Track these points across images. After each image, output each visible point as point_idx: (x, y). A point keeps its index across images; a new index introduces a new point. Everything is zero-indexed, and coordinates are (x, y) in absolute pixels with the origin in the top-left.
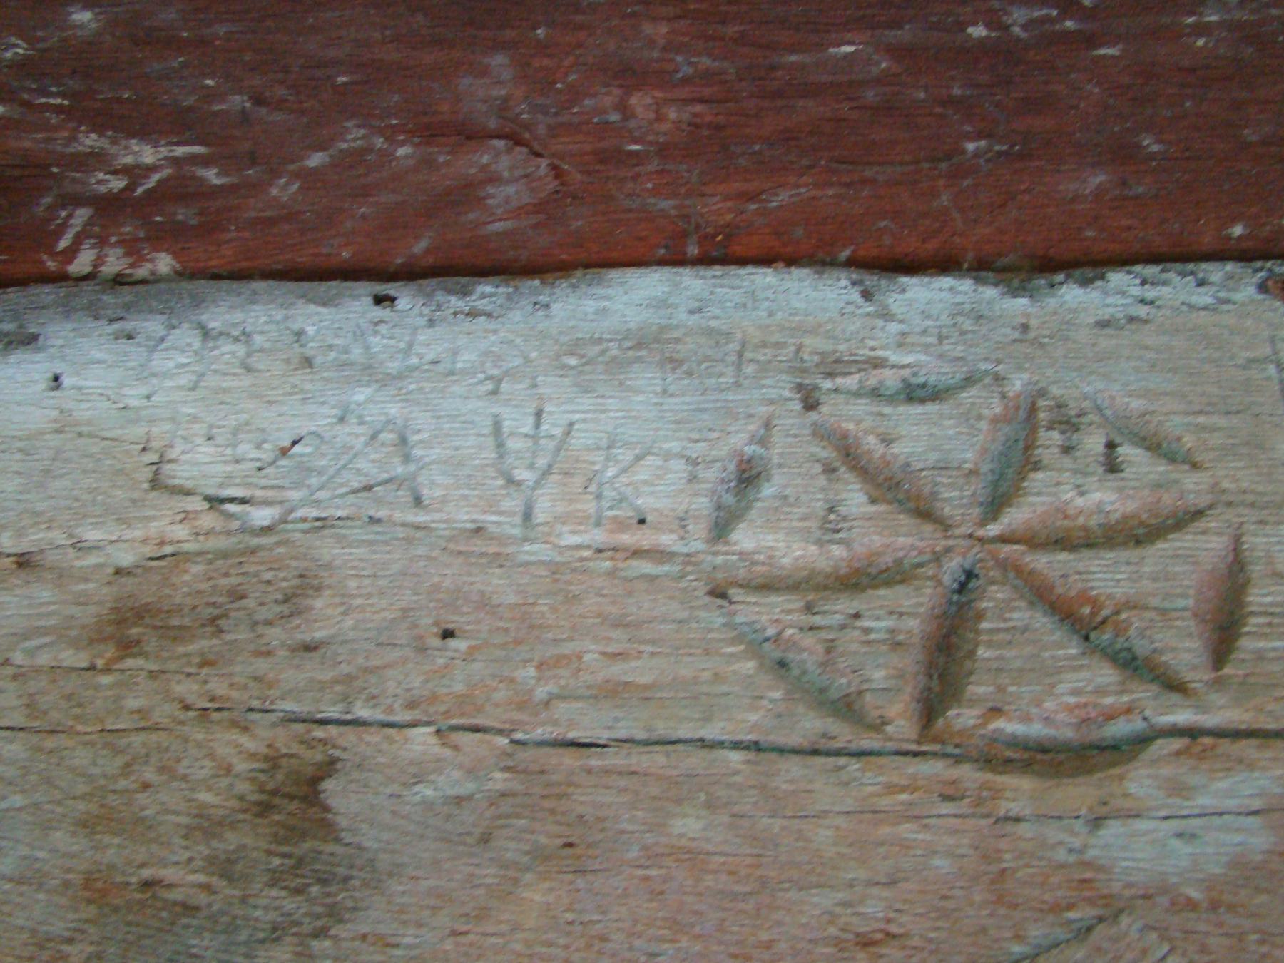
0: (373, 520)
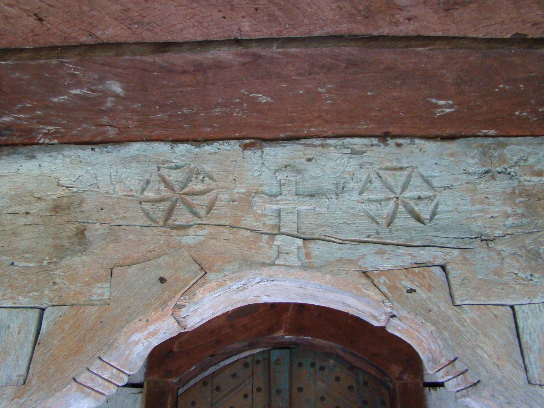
0: (92, 191)
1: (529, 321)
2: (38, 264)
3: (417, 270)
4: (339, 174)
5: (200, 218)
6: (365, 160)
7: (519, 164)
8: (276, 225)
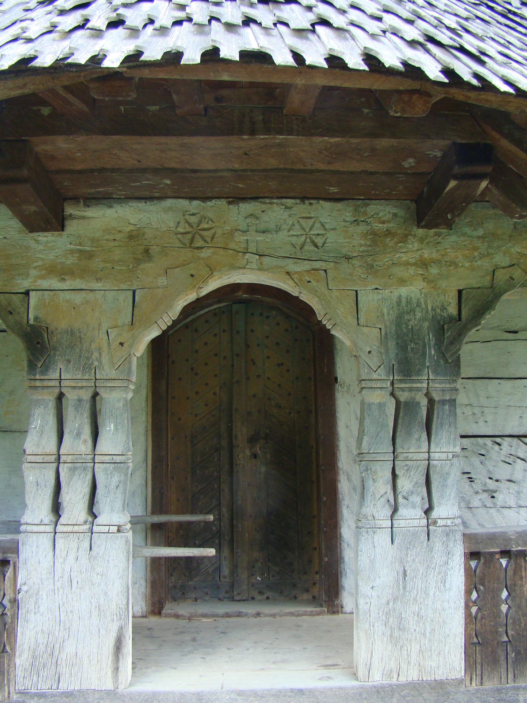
1: (363, 298)
2: (127, 268)
3: (312, 272)
4: (278, 220)
5: (208, 243)
6: (292, 212)
7: (374, 216)
8: (246, 248)
